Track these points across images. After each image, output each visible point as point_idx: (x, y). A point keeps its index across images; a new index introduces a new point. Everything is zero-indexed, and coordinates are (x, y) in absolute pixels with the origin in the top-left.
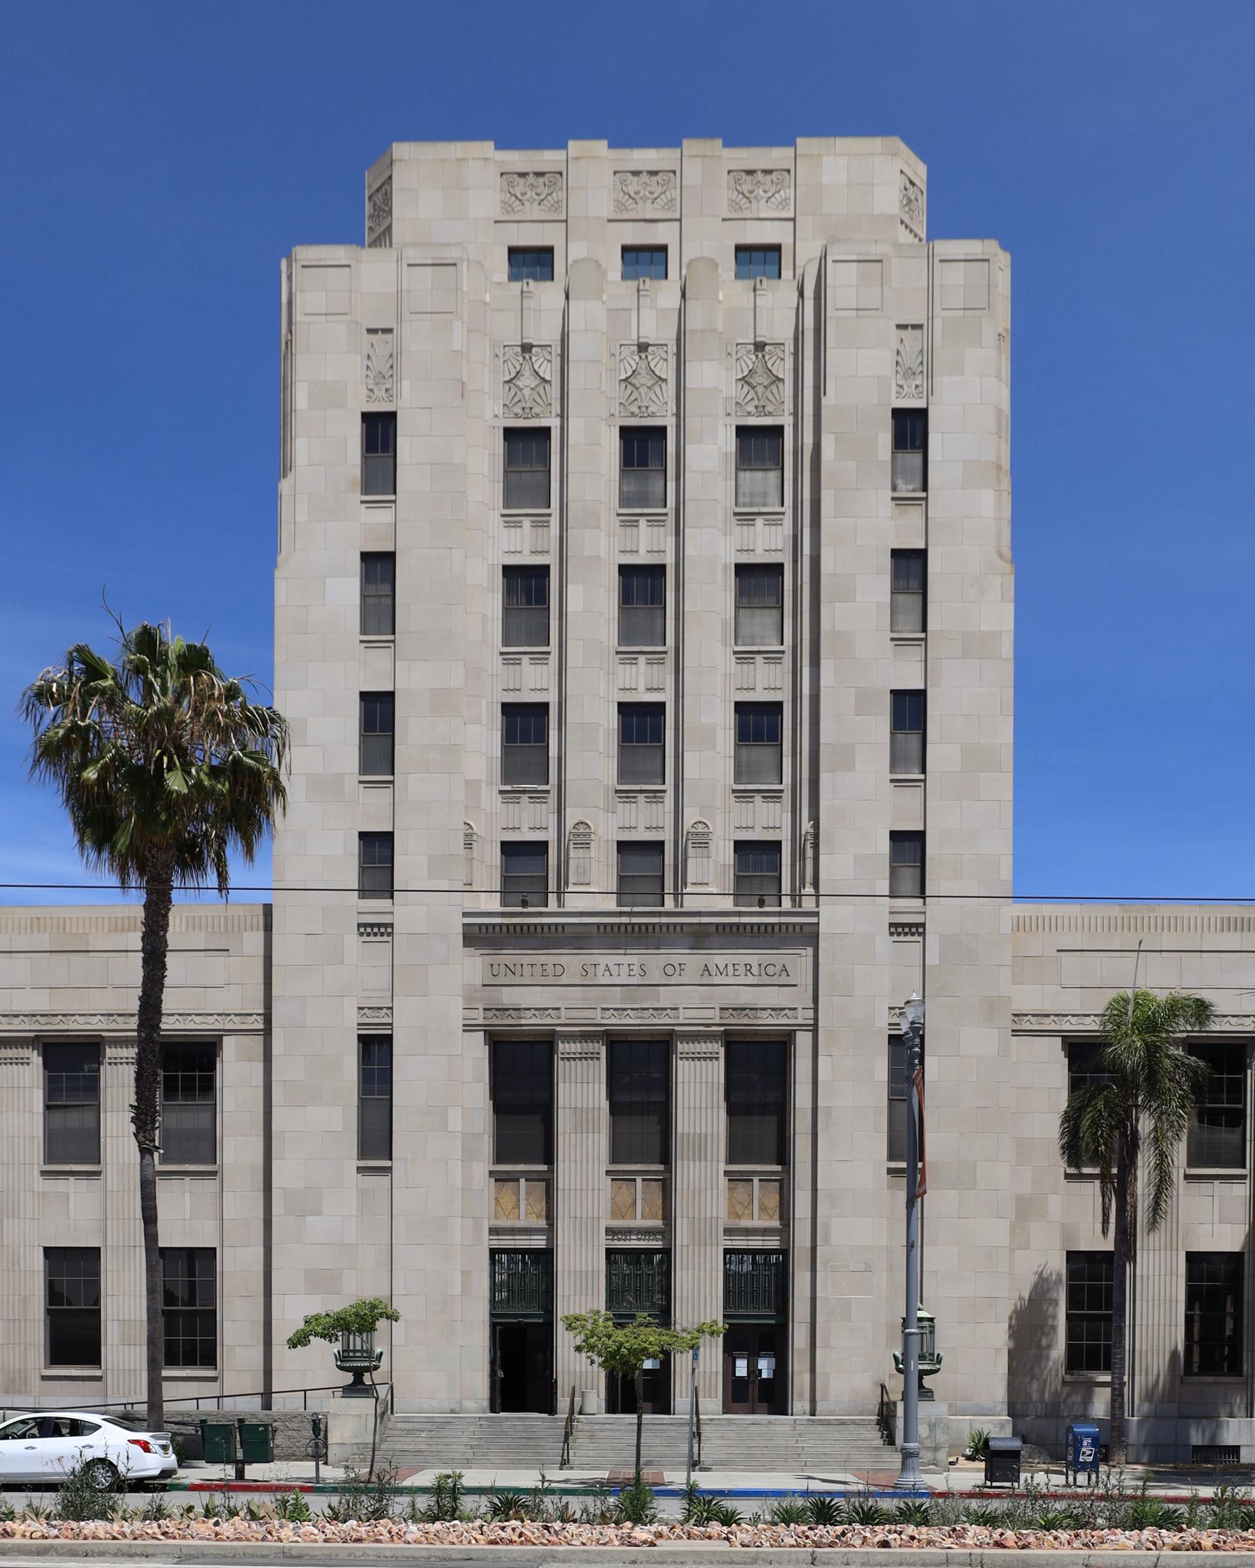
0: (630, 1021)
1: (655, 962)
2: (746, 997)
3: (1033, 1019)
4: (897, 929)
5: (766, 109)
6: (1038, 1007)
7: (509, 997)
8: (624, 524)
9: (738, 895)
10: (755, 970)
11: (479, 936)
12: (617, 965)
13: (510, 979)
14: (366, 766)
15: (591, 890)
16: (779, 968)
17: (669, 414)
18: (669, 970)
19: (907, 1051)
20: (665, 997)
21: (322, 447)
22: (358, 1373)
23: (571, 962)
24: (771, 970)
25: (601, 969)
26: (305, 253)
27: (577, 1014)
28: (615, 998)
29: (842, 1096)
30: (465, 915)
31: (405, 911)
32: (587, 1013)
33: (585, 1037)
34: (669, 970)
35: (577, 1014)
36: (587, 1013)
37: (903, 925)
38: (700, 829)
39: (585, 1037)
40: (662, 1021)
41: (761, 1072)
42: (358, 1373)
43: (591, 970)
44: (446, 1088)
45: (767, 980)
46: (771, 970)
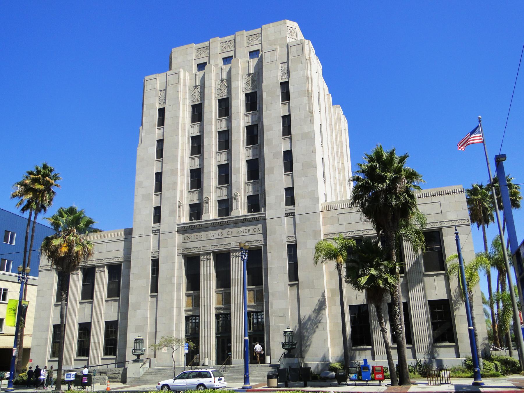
0: (218, 248)
1: (225, 232)
2: (249, 238)
3: (432, 224)
4: (288, 215)
5: (255, 20)
6: (332, 231)
7: (188, 245)
8: (219, 122)
9: (249, 211)
10: (251, 231)
11: (183, 230)
12: (215, 234)
13: (189, 240)
14: (156, 191)
15: (211, 213)
16: (257, 229)
17: (279, 61)
18: (229, 233)
19: (292, 249)
20: (227, 241)
21: (151, 116)
22: (138, 356)
23: (204, 234)
24: (255, 230)
25: (211, 235)
26: (147, 78)
27: (205, 248)
28: (215, 242)
29: (276, 264)
30: (177, 225)
31: (163, 226)
32: (208, 247)
33: (208, 254)
34: (229, 233)
35: (205, 248)
36: (208, 247)
37: (289, 213)
38: (236, 194)
39: (208, 254)
40: (438, 225)
41: (255, 260)
42: (138, 356)
43: (209, 235)
44: (175, 273)
45: (254, 233)
46: (255, 230)
